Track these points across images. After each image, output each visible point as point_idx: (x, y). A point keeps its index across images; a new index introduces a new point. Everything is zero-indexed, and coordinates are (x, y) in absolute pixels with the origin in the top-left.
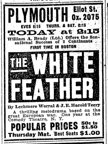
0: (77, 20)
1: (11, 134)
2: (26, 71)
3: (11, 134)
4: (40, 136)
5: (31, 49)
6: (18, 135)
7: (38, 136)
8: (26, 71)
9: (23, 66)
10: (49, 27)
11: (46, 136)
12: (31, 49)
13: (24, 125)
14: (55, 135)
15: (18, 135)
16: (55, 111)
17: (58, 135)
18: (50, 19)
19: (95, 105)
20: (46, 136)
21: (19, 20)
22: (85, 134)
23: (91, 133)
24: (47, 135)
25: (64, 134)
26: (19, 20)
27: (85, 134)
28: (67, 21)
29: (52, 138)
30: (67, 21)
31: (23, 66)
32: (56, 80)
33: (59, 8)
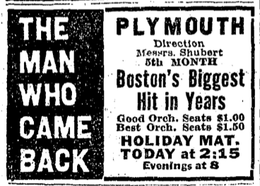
0: (211, 74)
1: (226, 23)
2: (26, 37)
3: (128, 153)
4: (173, 33)
5: (119, 33)
6: (177, 167)
7: (166, 33)
8: (26, 37)
9: (56, 38)
10: (234, 32)
11: (187, 158)
12: (119, 33)
13: (193, 73)
14: (191, 85)
15: (177, 167)
16: (167, 43)
17: (224, 85)
18: (206, 29)
19: (161, 117)
20: (187, 158)
21: (139, 30)
22: (220, 157)
23: (232, 118)
24: (189, 155)
25: (194, 155)
26: (139, 30)
27: (220, 157)
28: (243, 33)
29: (250, 21)
30: (243, 33)
31: (56, 38)
32: (31, 20)
33: (227, 19)
